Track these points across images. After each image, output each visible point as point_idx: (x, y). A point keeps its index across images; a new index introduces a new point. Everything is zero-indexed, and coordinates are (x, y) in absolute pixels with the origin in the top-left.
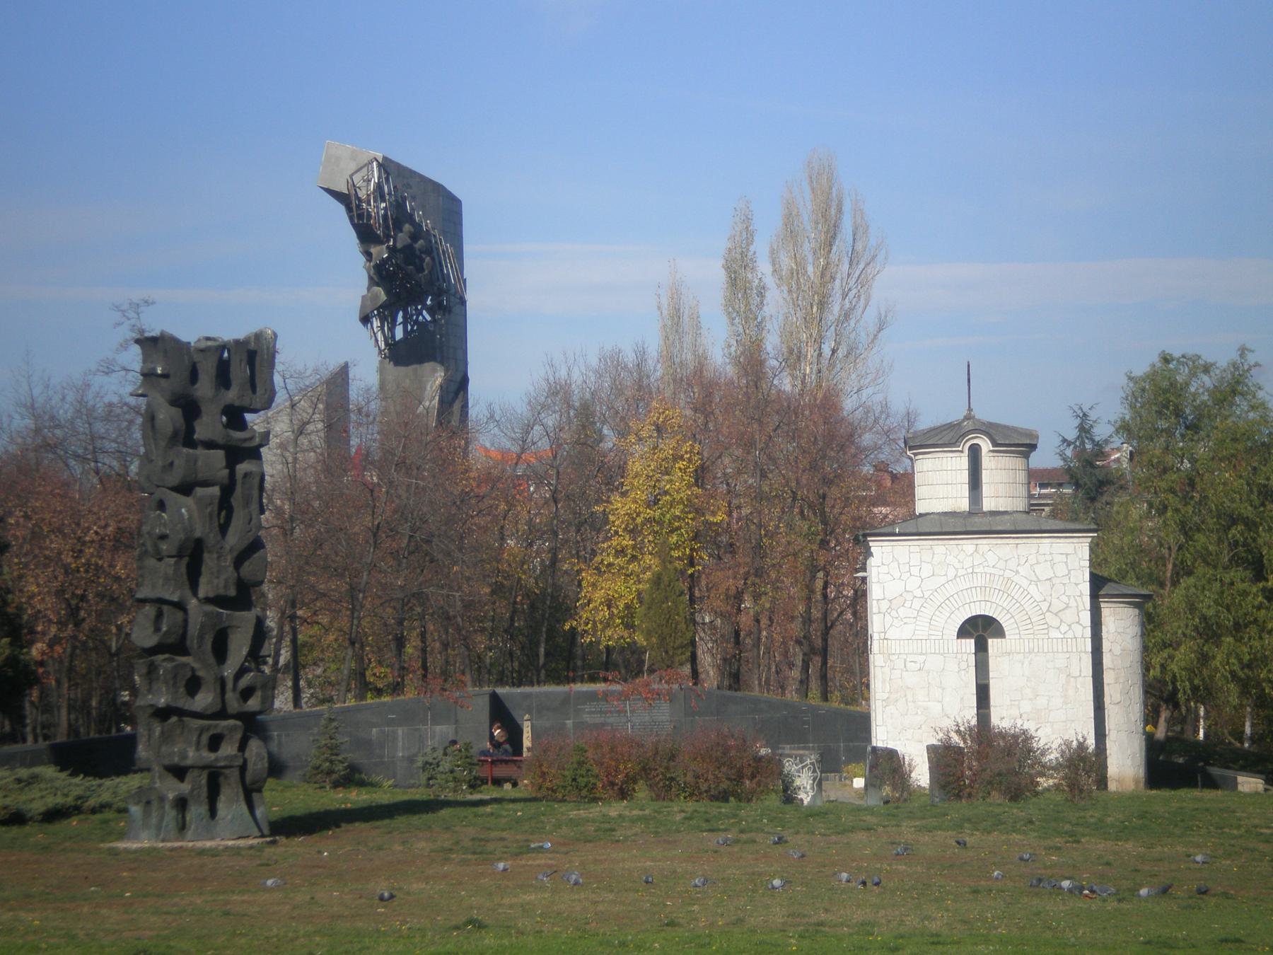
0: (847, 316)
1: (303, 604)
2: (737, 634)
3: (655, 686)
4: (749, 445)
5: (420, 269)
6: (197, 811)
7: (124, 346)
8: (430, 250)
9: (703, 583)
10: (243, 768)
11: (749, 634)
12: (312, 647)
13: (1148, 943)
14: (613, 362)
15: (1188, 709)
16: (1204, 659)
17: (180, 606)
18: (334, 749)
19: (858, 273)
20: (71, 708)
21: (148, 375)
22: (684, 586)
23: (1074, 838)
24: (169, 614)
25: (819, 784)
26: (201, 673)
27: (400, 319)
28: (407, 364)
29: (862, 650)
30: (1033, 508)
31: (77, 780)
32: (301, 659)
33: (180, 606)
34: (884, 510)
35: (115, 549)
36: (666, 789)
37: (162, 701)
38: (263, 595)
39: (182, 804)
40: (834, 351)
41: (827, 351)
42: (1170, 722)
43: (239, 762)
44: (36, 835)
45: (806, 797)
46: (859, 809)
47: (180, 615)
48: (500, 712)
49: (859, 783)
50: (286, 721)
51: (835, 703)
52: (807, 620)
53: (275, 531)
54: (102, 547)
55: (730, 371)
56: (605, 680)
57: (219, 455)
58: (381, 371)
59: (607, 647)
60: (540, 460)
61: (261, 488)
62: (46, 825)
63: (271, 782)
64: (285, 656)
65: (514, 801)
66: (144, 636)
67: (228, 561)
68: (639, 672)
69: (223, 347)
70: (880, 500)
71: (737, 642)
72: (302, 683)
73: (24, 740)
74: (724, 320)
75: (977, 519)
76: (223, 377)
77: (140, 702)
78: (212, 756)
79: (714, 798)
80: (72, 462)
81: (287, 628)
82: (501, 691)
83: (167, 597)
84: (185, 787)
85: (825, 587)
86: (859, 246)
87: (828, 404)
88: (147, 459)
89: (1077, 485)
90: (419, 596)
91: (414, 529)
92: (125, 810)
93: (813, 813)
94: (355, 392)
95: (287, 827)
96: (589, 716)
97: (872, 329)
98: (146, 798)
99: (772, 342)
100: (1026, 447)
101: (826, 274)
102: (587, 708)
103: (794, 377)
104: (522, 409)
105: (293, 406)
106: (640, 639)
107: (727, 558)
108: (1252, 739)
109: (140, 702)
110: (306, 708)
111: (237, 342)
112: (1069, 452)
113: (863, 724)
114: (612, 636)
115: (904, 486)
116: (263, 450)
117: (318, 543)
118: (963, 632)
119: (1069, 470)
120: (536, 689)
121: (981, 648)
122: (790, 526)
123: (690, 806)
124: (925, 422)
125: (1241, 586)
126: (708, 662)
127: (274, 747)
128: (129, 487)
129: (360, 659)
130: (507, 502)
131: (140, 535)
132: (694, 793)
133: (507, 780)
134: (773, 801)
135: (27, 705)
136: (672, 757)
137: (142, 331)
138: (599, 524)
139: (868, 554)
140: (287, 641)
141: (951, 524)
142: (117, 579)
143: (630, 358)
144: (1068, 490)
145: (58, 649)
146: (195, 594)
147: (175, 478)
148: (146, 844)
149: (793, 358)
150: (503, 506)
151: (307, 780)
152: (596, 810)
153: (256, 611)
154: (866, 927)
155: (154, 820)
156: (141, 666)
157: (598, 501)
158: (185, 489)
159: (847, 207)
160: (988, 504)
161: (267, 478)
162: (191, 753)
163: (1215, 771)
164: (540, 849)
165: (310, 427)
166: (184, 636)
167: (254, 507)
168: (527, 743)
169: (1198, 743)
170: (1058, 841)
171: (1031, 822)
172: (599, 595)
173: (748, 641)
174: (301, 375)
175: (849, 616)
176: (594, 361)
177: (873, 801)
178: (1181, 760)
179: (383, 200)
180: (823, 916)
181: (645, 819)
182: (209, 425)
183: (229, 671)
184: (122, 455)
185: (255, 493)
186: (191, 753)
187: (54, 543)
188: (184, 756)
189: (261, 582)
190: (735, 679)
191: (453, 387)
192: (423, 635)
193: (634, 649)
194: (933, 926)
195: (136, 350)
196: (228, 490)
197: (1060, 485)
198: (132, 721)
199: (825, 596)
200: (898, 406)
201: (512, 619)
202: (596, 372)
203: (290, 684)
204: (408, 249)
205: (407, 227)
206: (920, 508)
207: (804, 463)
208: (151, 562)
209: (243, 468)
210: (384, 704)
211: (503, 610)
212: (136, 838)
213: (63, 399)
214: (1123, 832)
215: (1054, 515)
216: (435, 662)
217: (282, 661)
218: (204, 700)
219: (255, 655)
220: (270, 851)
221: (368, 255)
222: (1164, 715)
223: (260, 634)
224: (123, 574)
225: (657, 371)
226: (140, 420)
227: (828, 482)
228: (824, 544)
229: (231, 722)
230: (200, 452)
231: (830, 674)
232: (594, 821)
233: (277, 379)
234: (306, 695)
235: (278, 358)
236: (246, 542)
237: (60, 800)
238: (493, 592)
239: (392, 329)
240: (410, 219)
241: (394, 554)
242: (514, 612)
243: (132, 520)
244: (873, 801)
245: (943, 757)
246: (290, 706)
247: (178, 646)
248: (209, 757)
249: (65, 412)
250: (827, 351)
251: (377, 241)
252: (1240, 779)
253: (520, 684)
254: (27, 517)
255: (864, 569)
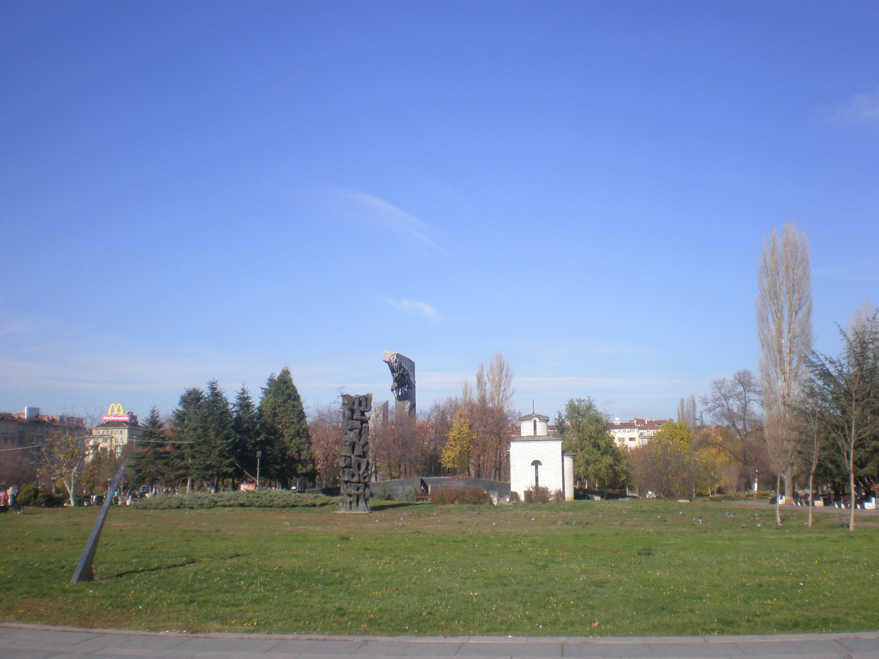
0: (505, 389)
1: (378, 457)
2: (479, 465)
3: (460, 477)
4: (482, 420)
5: (405, 379)
6: (354, 504)
7: (338, 397)
8: (407, 374)
9: (471, 452)
10: (364, 495)
11: (482, 465)
12: (380, 467)
13: (574, 536)
14: (450, 400)
15: (584, 482)
16: (587, 469)
17: (350, 457)
18: (385, 491)
19: (508, 379)
20: (326, 480)
21: (344, 404)
22: (466, 453)
23: (558, 512)
24: (348, 460)
25: (498, 500)
26: (355, 473)
27: (400, 390)
28: (401, 401)
29: (509, 469)
30: (548, 435)
31: (327, 497)
32: (377, 470)
33: (350, 457)
34: (514, 435)
35: (336, 444)
36: (462, 501)
37: (346, 479)
38: (368, 455)
39: (351, 503)
40: (502, 398)
41: (500, 398)
42: (580, 484)
43: (363, 494)
44: (318, 509)
45: (495, 503)
46: (508, 506)
47: (350, 459)
48: (423, 483)
49: (508, 500)
50: (374, 484)
51: (502, 481)
52: (496, 462)
53: (371, 440)
54: (333, 443)
55: (478, 402)
56: (448, 476)
57: (359, 422)
58: (396, 402)
59: (448, 468)
60: (432, 423)
61: (368, 430)
62: (320, 507)
63: (370, 499)
64: (373, 469)
65: (426, 504)
66: (342, 464)
67: (361, 447)
68: (456, 474)
69: (360, 397)
70: (513, 433)
71: (479, 467)
72: (378, 475)
73: (315, 487)
74: (477, 390)
75: (536, 437)
76: (360, 404)
77: (341, 479)
78: (357, 492)
79: (474, 504)
80: (327, 424)
81: (374, 462)
82: (423, 478)
83: (347, 455)
84: (351, 499)
85: (500, 453)
86: (508, 373)
87: (501, 410)
88: (343, 423)
89: (558, 429)
90: (404, 456)
91: (403, 440)
92: (338, 504)
93: (497, 507)
94: (389, 408)
95: (374, 509)
96: (444, 484)
97: (511, 393)
98: (343, 501)
99: (488, 396)
100: (547, 421)
101: (500, 380)
102: (443, 482)
103: (493, 404)
104: (428, 411)
105: (376, 411)
106: (456, 466)
107: (477, 447)
108: (598, 488)
109: (341, 479)
110: (378, 482)
111: (363, 396)
112: (556, 422)
113: (509, 486)
114: (449, 466)
115: (518, 430)
116: (369, 421)
117: (381, 443)
118: (532, 464)
119: (556, 426)
120: (431, 478)
121: (537, 468)
122: (492, 439)
123: (468, 505)
124: (523, 415)
125: (595, 452)
126: (472, 472)
127: (371, 490)
128: (339, 430)
129: (390, 470)
130: (425, 433)
131: (341, 440)
132: (469, 502)
133: (425, 499)
134: (488, 504)
135: (316, 479)
136: (464, 494)
137: (342, 394)
138: (446, 439)
139: (510, 445)
140: (374, 466)
141: (529, 439)
142: (336, 451)
143: (454, 399)
144: (556, 431)
145: (323, 467)
146: (353, 454)
147: (349, 427)
148: (343, 512)
149: (493, 399)
150: (423, 435)
151: (379, 498)
152: (446, 506)
153: (367, 458)
154: (510, 533)
155: (345, 507)
156: (341, 471)
157: (446, 433)
158: (351, 430)
159: (505, 364)
160: (538, 434)
161: (370, 428)
162: (353, 491)
163: (590, 495)
164: (433, 515)
165: (379, 416)
166: (351, 464)
167: (367, 434)
168: (429, 490)
169: (585, 490)
170: (554, 513)
171: (548, 508)
172: (446, 455)
173: (482, 467)
174: (378, 404)
175: (506, 460)
176: (445, 400)
177: (511, 504)
178: (582, 493)
179: (397, 363)
180: (499, 531)
181: (457, 508)
182: (357, 415)
183: (361, 472)
184: (338, 422)
185: (367, 431)
186: (353, 491)
187: (322, 442)
188: (351, 492)
189: (368, 452)
190: (478, 475)
191: (412, 406)
192: (405, 465)
193: (455, 469)
194: (525, 533)
195: (341, 398)
196: (361, 430)
197: (554, 429)
198: (339, 483)
199: (500, 456)
200: (517, 411)
201: (426, 461)
202: (446, 403)
203: (375, 476)
204: (402, 374)
205: (402, 369)
206: (522, 435)
207: (495, 424)
208: (344, 447)
209: (364, 425)
210: (396, 481)
211: (423, 459)
212: (341, 510)
213: (325, 409)
214: (569, 510)
215: (553, 436)
216: (408, 471)
217: (373, 470)
218: (356, 479)
219: (367, 469)
220: (371, 514)
221: (393, 376)
222: (578, 483)
223: (368, 464)
224: (337, 450)
225: (460, 402)
226: (341, 414)
227: (501, 429)
228: (500, 443)
229: (361, 484)
230: (355, 421)
231: (501, 474)
232: (445, 509)
233: (372, 404)
234: (378, 479)
235: (372, 400)
236: (365, 443)
237: (323, 501)
238: (422, 455)
239: (398, 393)
240: (403, 367)
241: (399, 446)
242: (426, 459)
243: (339, 437)
244: (511, 504)
245: (528, 494)
246: (375, 481)
247: (349, 466)
248: (357, 492)
249: (326, 412)
250: (500, 398)
251: (396, 372)
252: (595, 497)
253: (428, 476)
254: (316, 436)
255: (509, 449)
